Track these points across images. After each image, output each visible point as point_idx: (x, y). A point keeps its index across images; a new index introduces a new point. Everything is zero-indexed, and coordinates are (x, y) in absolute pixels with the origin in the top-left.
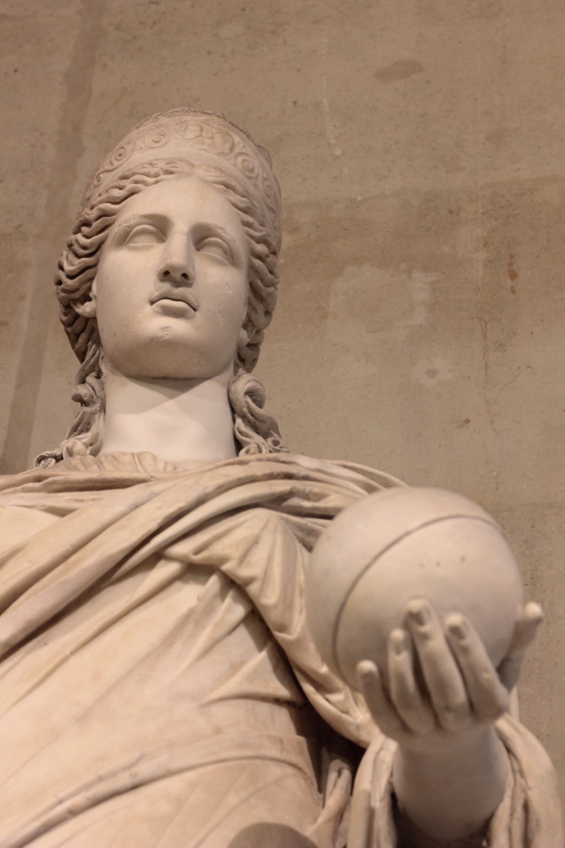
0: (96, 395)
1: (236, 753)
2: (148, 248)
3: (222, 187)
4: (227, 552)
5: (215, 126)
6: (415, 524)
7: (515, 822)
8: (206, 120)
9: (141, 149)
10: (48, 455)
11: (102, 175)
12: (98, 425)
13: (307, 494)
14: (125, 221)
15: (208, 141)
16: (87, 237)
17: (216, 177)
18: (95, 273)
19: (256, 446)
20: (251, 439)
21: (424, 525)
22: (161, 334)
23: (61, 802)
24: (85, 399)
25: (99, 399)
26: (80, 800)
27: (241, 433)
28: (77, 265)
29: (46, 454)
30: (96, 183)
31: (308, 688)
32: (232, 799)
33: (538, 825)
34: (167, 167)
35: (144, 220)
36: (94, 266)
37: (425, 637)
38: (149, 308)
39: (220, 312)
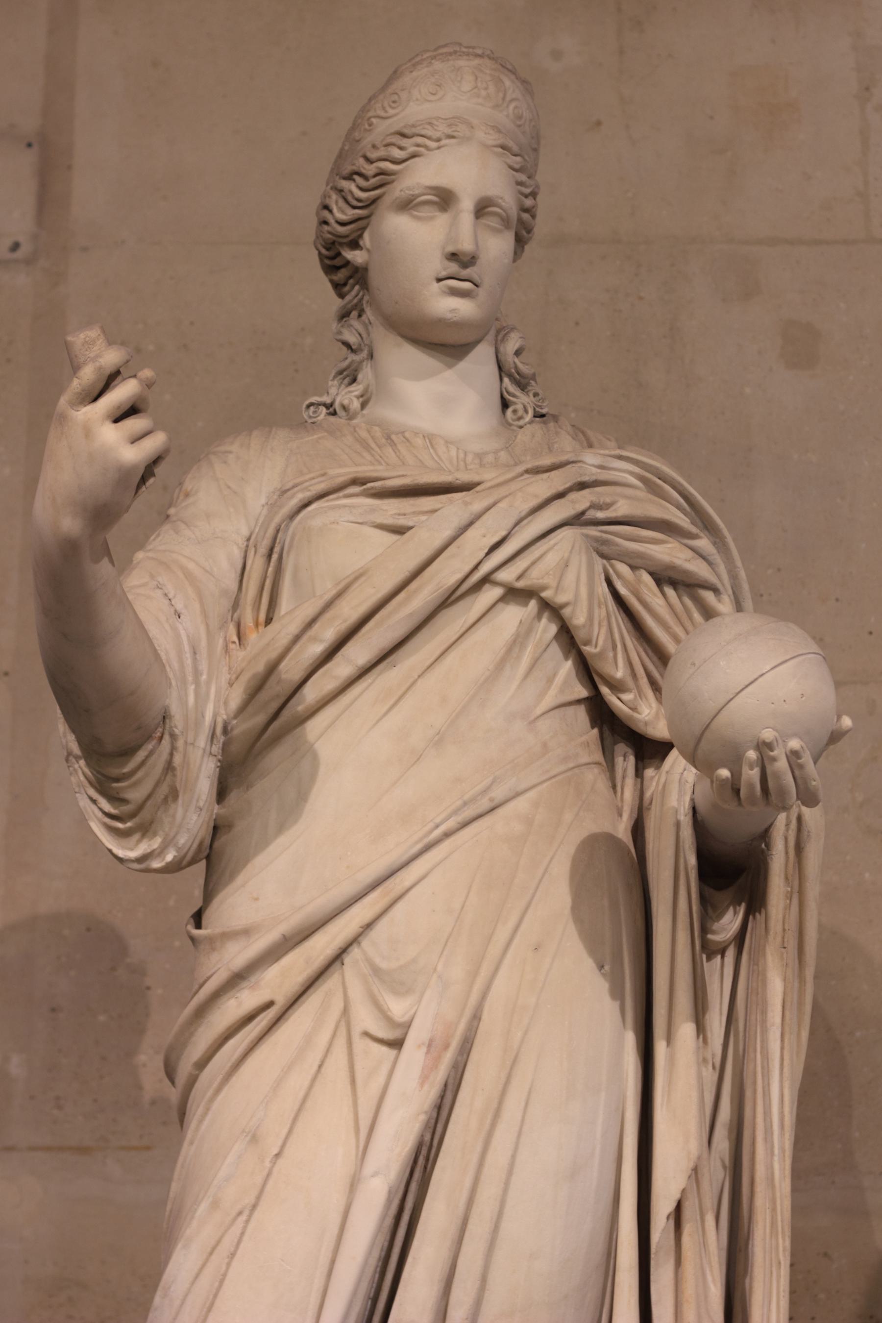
0: (364, 343)
1: (562, 768)
2: (432, 218)
3: (500, 150)
4: (545, 581)
5: (488, 72)
6: (768, 668)
7: (790, 832)
8: (479, 65)
9: (417, 100)
10: (318, 401)
11: (374, 120)
12: (366, 375)
13: (601, 506)
14: (409, 189)
15: (483, 93)
16: (362, 189)
17: (495, 140)
18: (368, 225)
19: (522, 407)
20: (517, 399)
21: (772, 669)
22: (449, 316)
23: (437, 826)
24: (354, 347)
25: (367, 347)
26: (451, 824)
27: (507, 392)
28: (349, 215)
29: (316, 400)
30: (367, 126)
31: (605, 690)
32: (568, 817)
33: (808, 836)
34: (449, 131)
35: (429, 191)
36: (368, 217)
37: (774, 759)
38: (436, 286)
39: (498, 284)
